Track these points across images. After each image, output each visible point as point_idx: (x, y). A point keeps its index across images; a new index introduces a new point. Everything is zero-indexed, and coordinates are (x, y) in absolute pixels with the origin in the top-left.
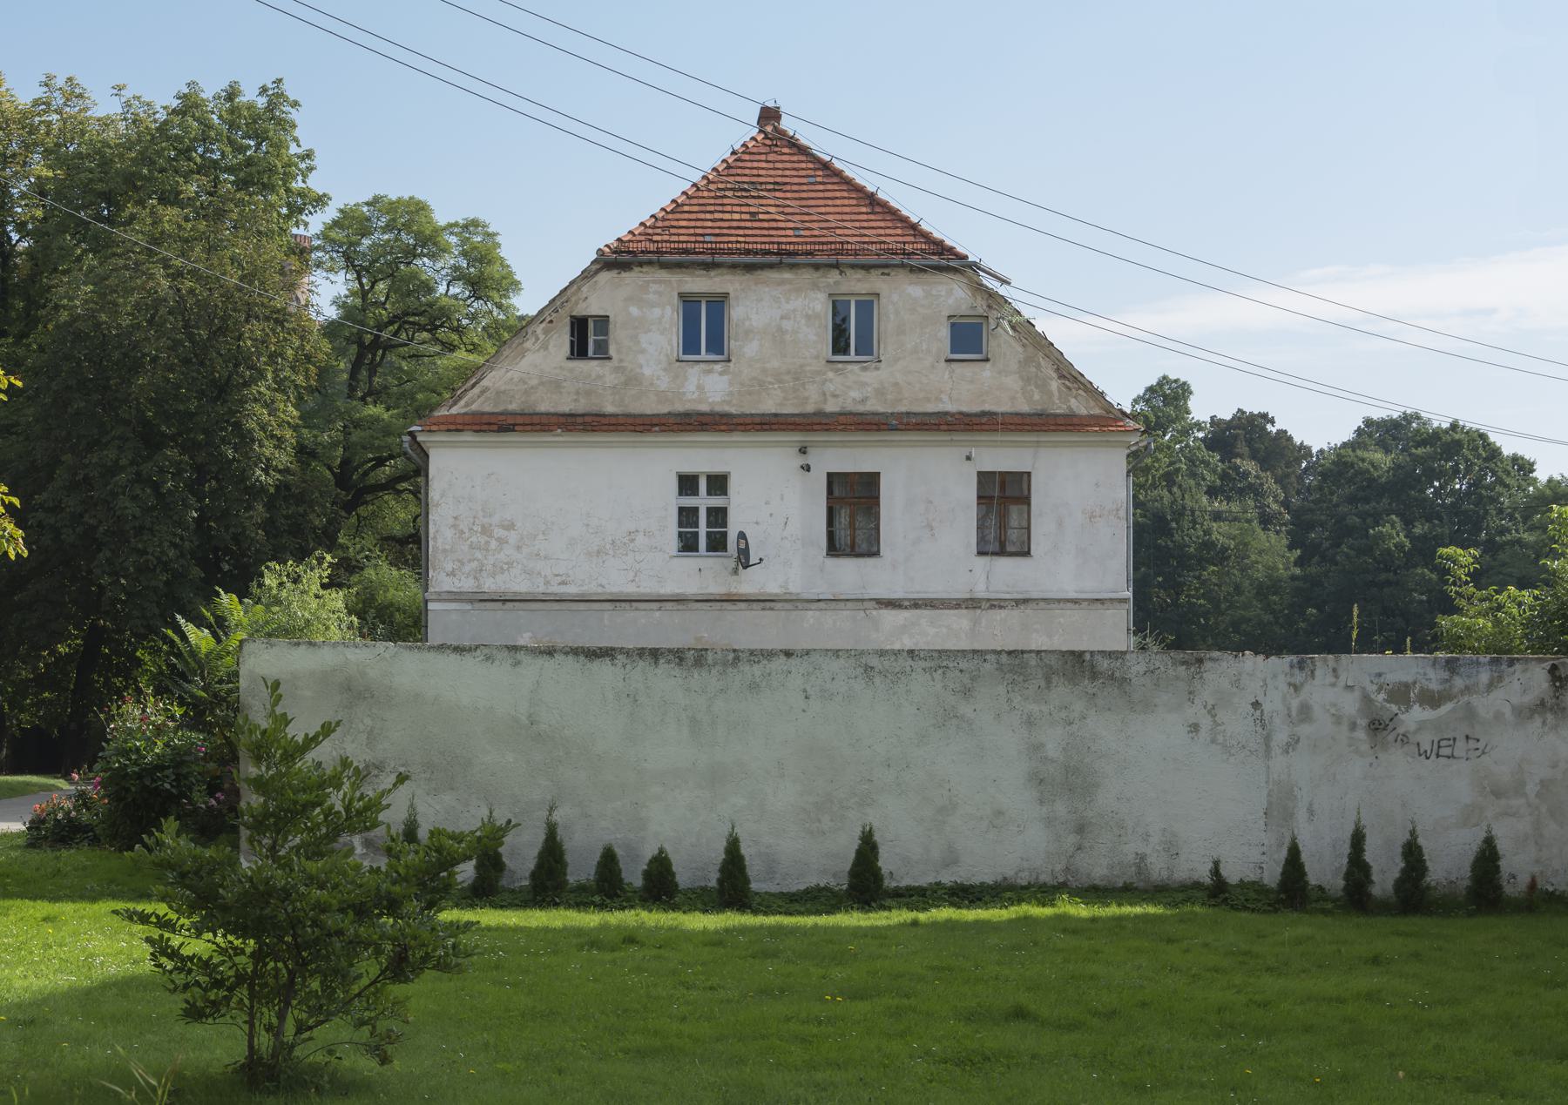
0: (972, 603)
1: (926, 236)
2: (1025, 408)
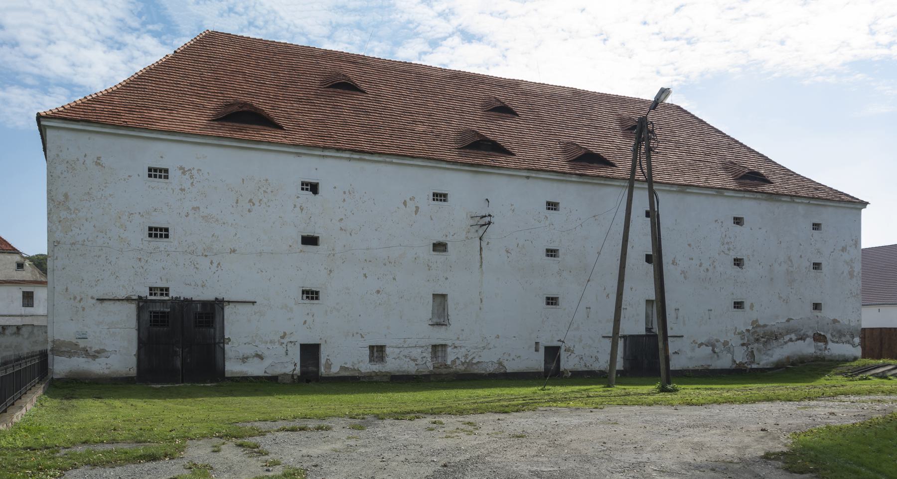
0: (21, 316)
1: (12, 247)
2: (32, 280)
